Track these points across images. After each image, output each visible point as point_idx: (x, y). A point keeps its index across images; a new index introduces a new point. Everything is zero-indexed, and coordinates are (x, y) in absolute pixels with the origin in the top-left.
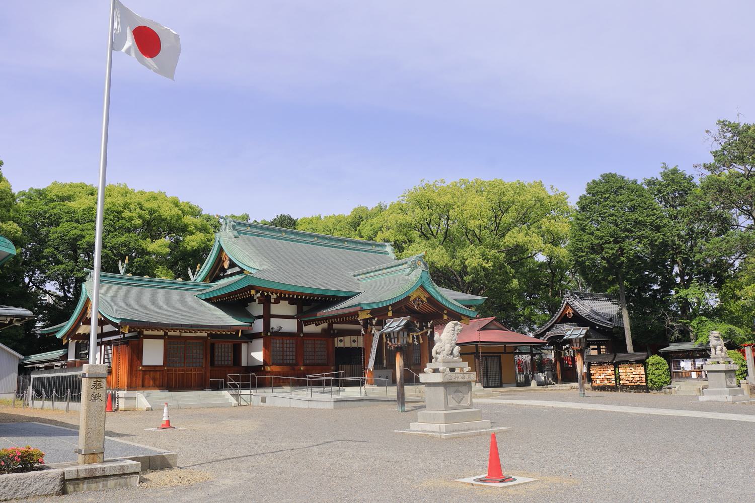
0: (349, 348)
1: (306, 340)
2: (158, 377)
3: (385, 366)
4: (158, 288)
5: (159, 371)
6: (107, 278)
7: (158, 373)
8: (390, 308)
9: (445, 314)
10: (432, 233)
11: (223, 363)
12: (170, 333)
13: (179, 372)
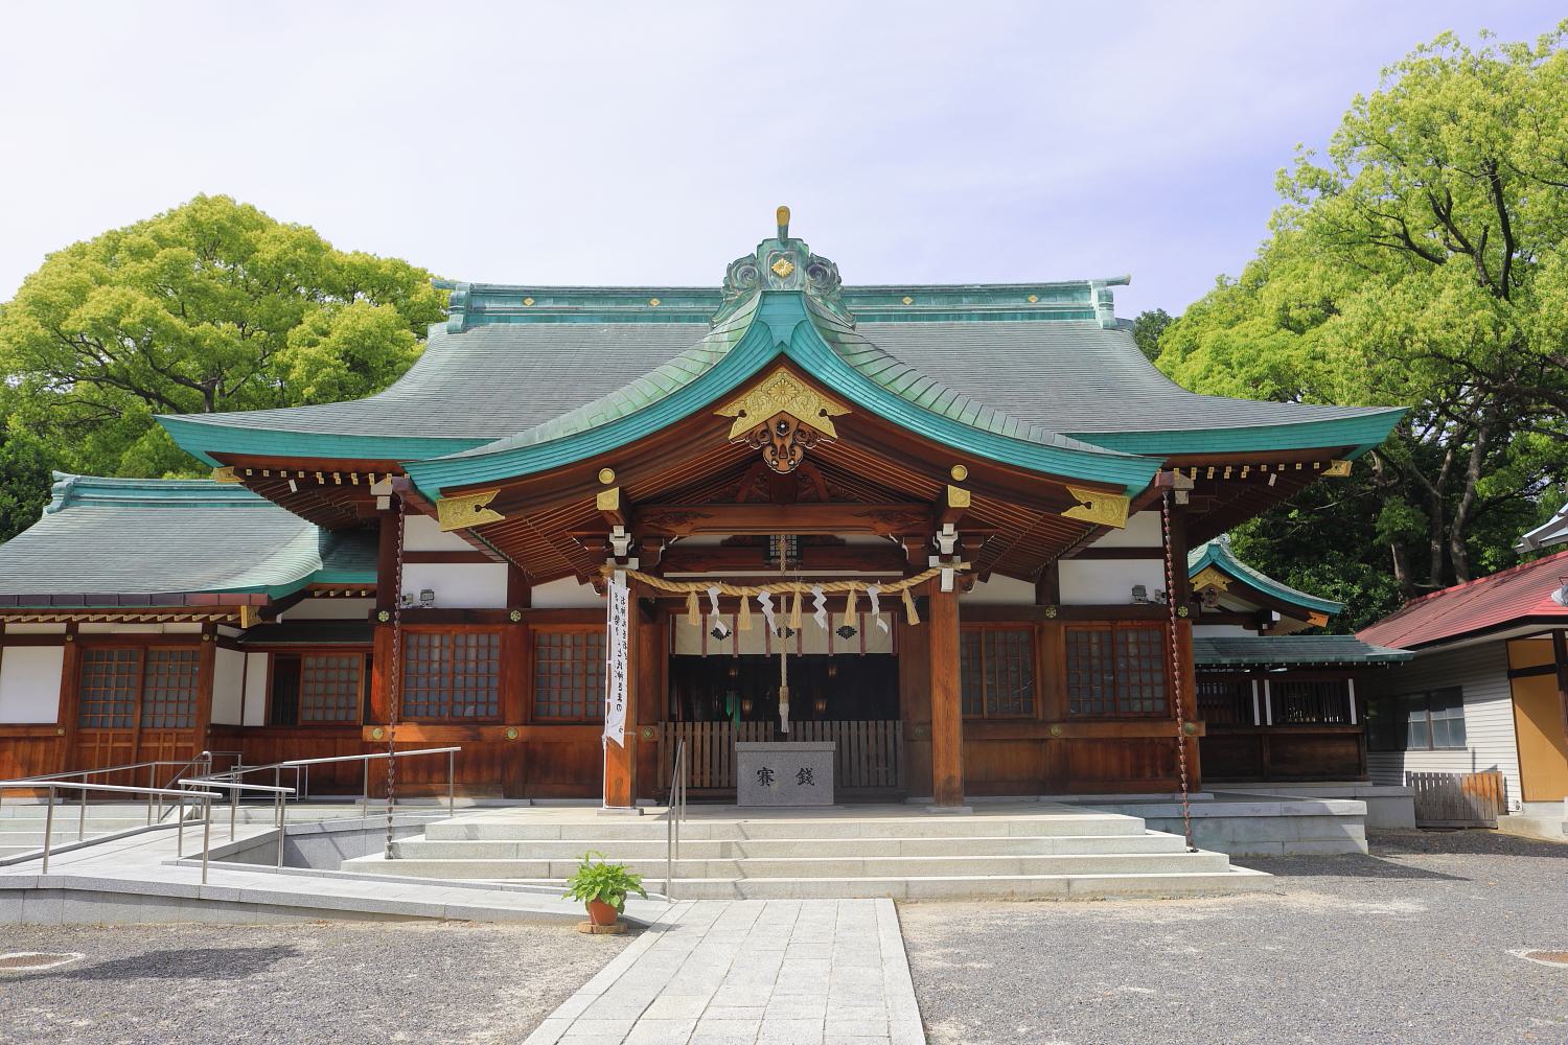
0: (856, 656)
1: (415, 632)
2: (41, 758)
3: (785, 727)
4: (233, 505)
5: (47, 739)
6: (198, 493)
7: (42, 746)
8: (607, 476)
9: (958, 484)
10: (1464, 242)
11: (1147, 704)
12: (84, 628)
13: (117, 745)
